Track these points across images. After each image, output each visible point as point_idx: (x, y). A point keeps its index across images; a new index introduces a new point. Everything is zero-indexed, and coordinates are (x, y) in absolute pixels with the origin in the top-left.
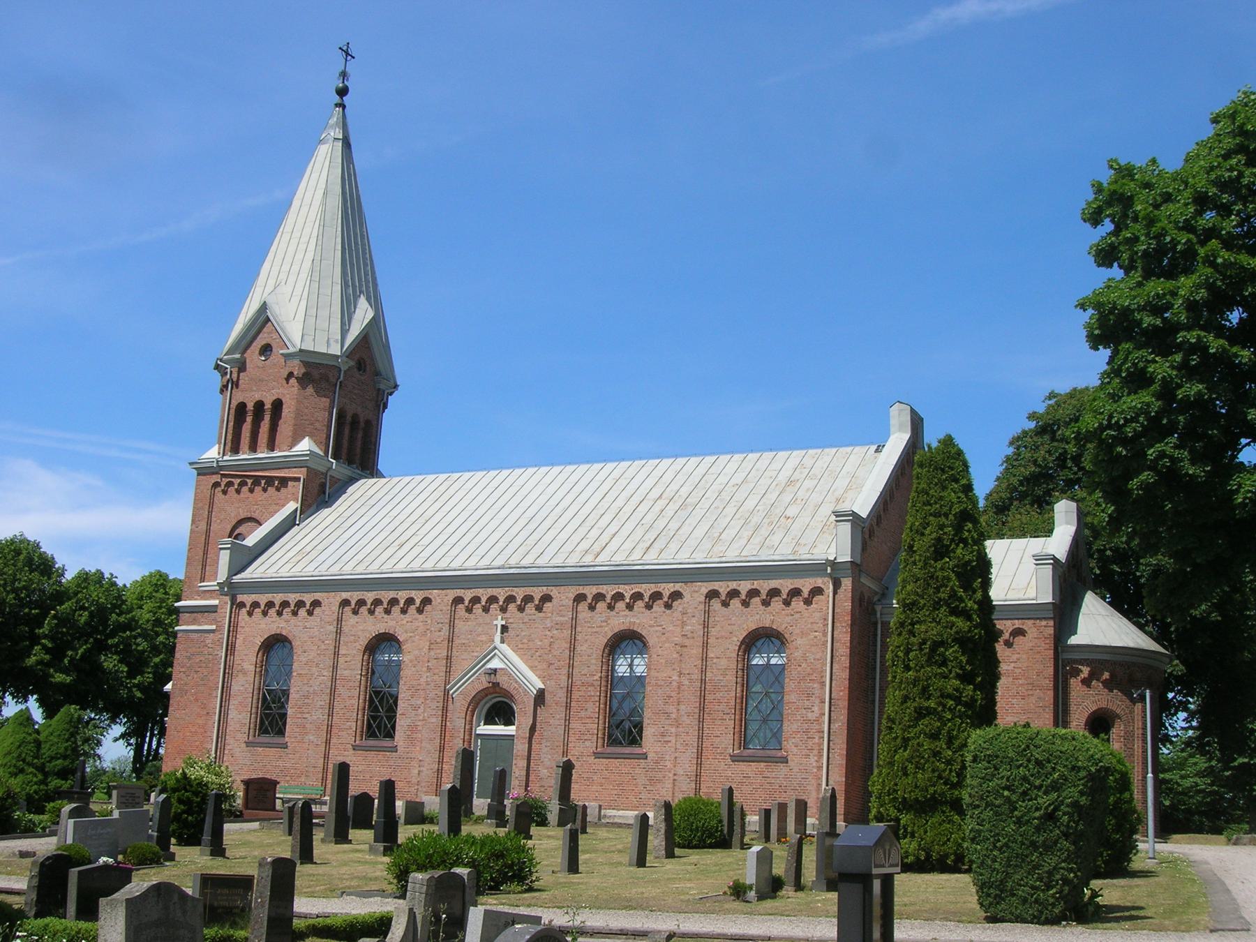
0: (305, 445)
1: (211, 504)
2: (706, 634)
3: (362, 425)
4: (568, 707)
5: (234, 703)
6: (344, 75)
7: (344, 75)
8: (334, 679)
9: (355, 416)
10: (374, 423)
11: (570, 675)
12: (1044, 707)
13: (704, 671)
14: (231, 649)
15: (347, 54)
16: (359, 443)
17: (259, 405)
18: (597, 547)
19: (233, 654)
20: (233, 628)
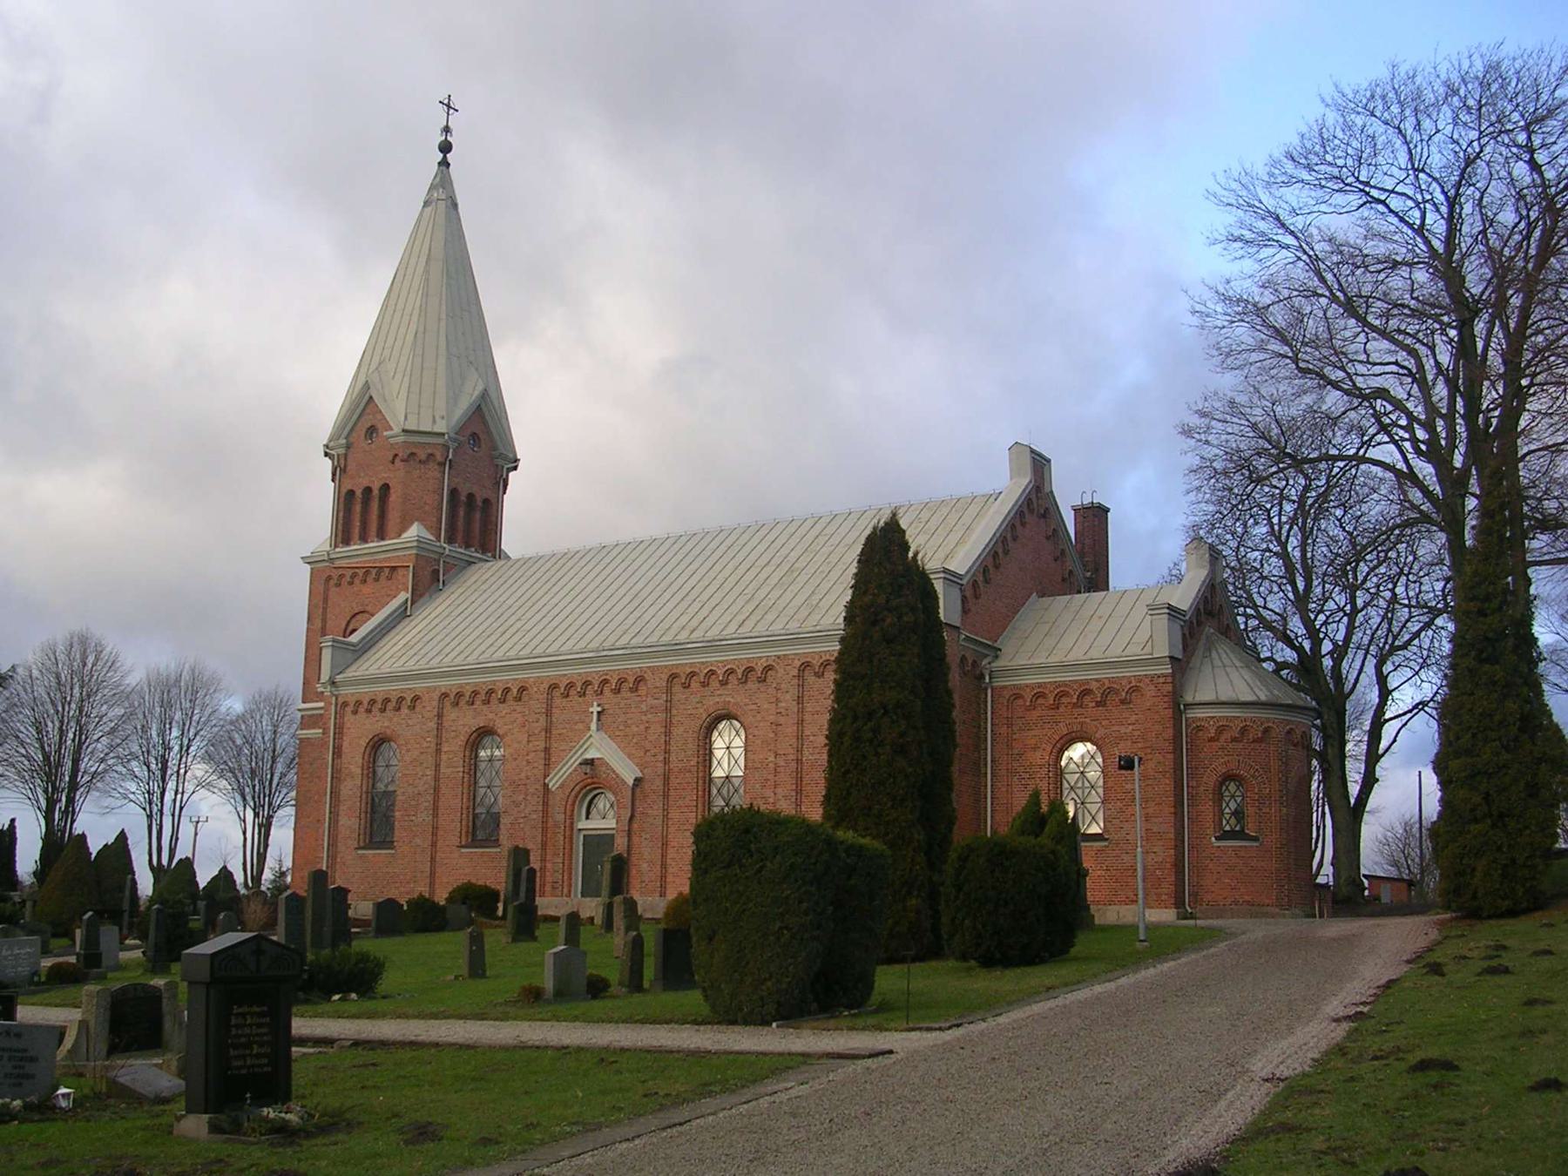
0: (414, 531)
1: (326, 600)
2: (801, 711)
3: (479, 503)
4: (666, 795)
5: (343, 808)
6: (447, 130)
7: (447, 130)
8: (437, 779)
9: (471, 496)
10: (494, 501)
11: (666, 762)
12: (1164, 773)
13: (799, 750)
14: (338, 752)
15: (449, 107)
16: (477, 526)
17: (368, 490)
18: (694, 623)
19: (340, 756)
20: (339, 731)
